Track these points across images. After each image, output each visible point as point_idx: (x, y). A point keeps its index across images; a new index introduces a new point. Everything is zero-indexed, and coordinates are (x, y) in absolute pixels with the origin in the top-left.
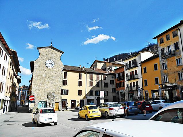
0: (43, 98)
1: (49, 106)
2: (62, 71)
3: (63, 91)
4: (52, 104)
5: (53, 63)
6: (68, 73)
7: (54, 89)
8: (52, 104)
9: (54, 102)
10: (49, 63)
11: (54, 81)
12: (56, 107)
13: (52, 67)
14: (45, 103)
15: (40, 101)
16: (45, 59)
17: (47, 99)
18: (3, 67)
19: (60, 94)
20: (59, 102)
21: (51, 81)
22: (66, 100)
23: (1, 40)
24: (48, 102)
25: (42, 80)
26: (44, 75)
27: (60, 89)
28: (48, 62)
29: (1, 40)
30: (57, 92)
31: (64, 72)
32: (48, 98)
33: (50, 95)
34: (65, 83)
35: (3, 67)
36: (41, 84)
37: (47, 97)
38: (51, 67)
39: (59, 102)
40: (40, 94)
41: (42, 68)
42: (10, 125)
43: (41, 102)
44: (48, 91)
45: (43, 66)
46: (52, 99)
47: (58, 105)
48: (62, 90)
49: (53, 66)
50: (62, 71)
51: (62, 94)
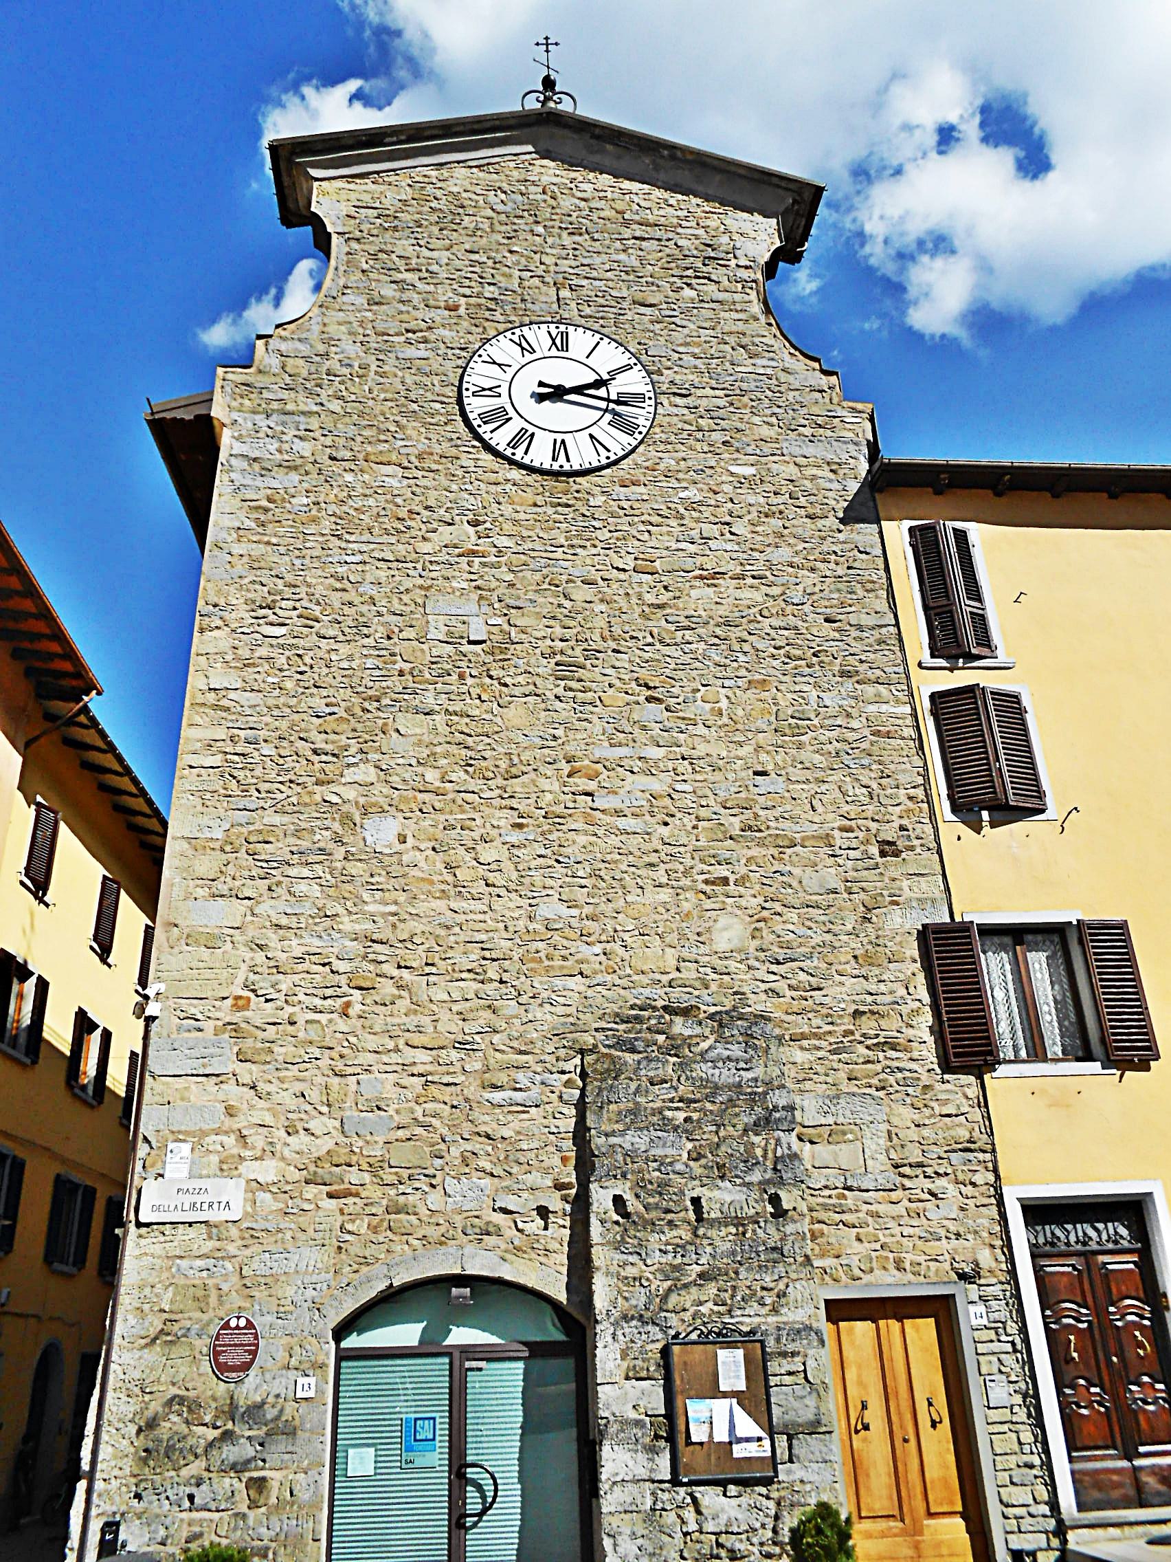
0: (467, 1194)
1: (670, 1429)
2: (861, 510)
3: (995, 967)
4: (731, 1367)
5: (633, 382)
6: (1002, 553)
7: (729, 932)
8: (758, 1370)
9: (805, 1305)
10: (526, 385)
11: (710, 746)
12: (875, 1447)
13: (617, 442)
14: (537, 1351)
15: (388, 1304)
16: (440, 315)
17: (581, 1206)
18: (81, 1015)
19: (929, 1052)
20: (941, 1309)
21: (617, 734)
22: (1133, 1211)
23: (10, 635)
24: (602, 1293)
25: (410, 724)
26: (458, 609)
27: (902, 925)
28: (510, 371)
29: (10, 635)
30: (842, 992)
31: (898, 533)
32: (601, 1198)
33: (659, 1086)
34: (987, 763)
35: (81, 1015)
36: (382, 833)
37: (585, 1164)
38: (582, 454)
39: (941, 1309)
40: (382, 1085)
41: (393, 478)
42: (912, 1371)
43: (407, 1334)
44: (572, 999)
45: (416, 438)
46: (722, 1197)
47: (929, 1379)
48: (949, 951)
49: (627, 426)
50: (861, 510)
51: (967, 1046)
